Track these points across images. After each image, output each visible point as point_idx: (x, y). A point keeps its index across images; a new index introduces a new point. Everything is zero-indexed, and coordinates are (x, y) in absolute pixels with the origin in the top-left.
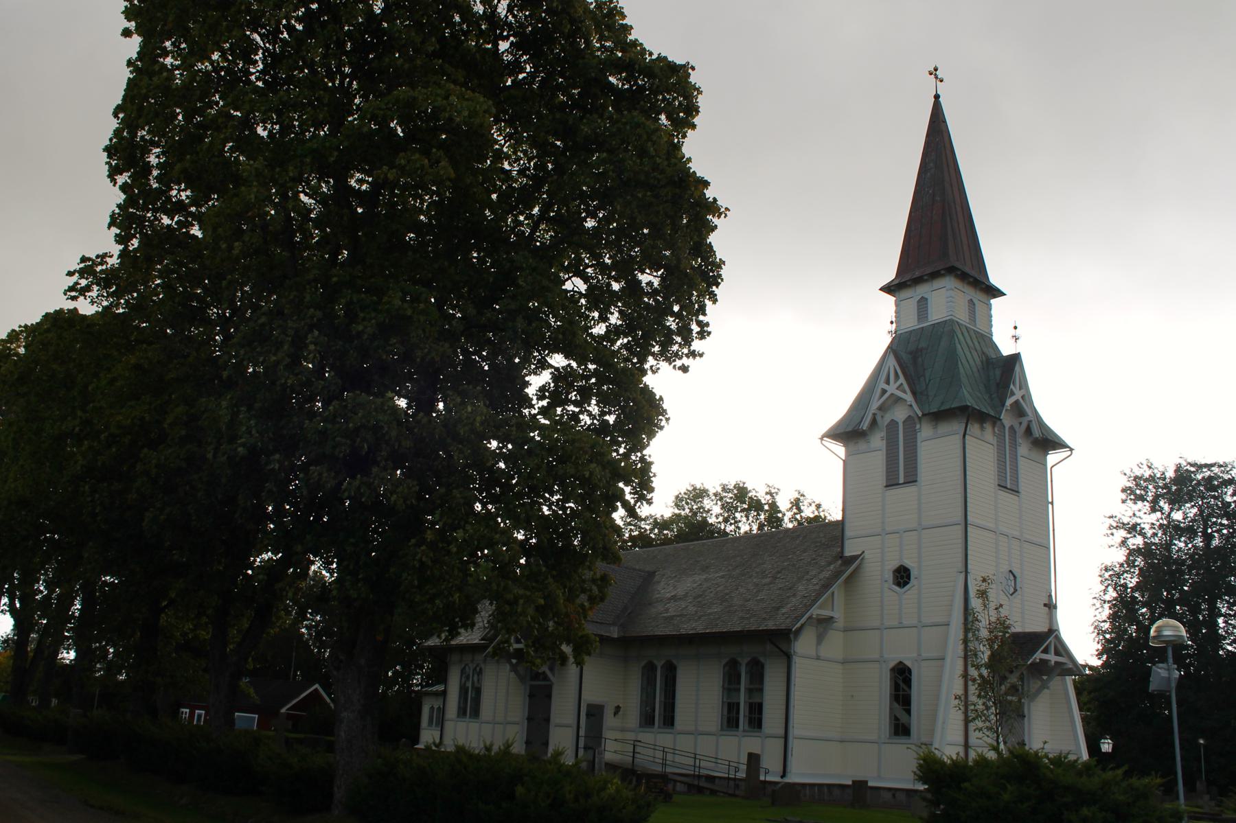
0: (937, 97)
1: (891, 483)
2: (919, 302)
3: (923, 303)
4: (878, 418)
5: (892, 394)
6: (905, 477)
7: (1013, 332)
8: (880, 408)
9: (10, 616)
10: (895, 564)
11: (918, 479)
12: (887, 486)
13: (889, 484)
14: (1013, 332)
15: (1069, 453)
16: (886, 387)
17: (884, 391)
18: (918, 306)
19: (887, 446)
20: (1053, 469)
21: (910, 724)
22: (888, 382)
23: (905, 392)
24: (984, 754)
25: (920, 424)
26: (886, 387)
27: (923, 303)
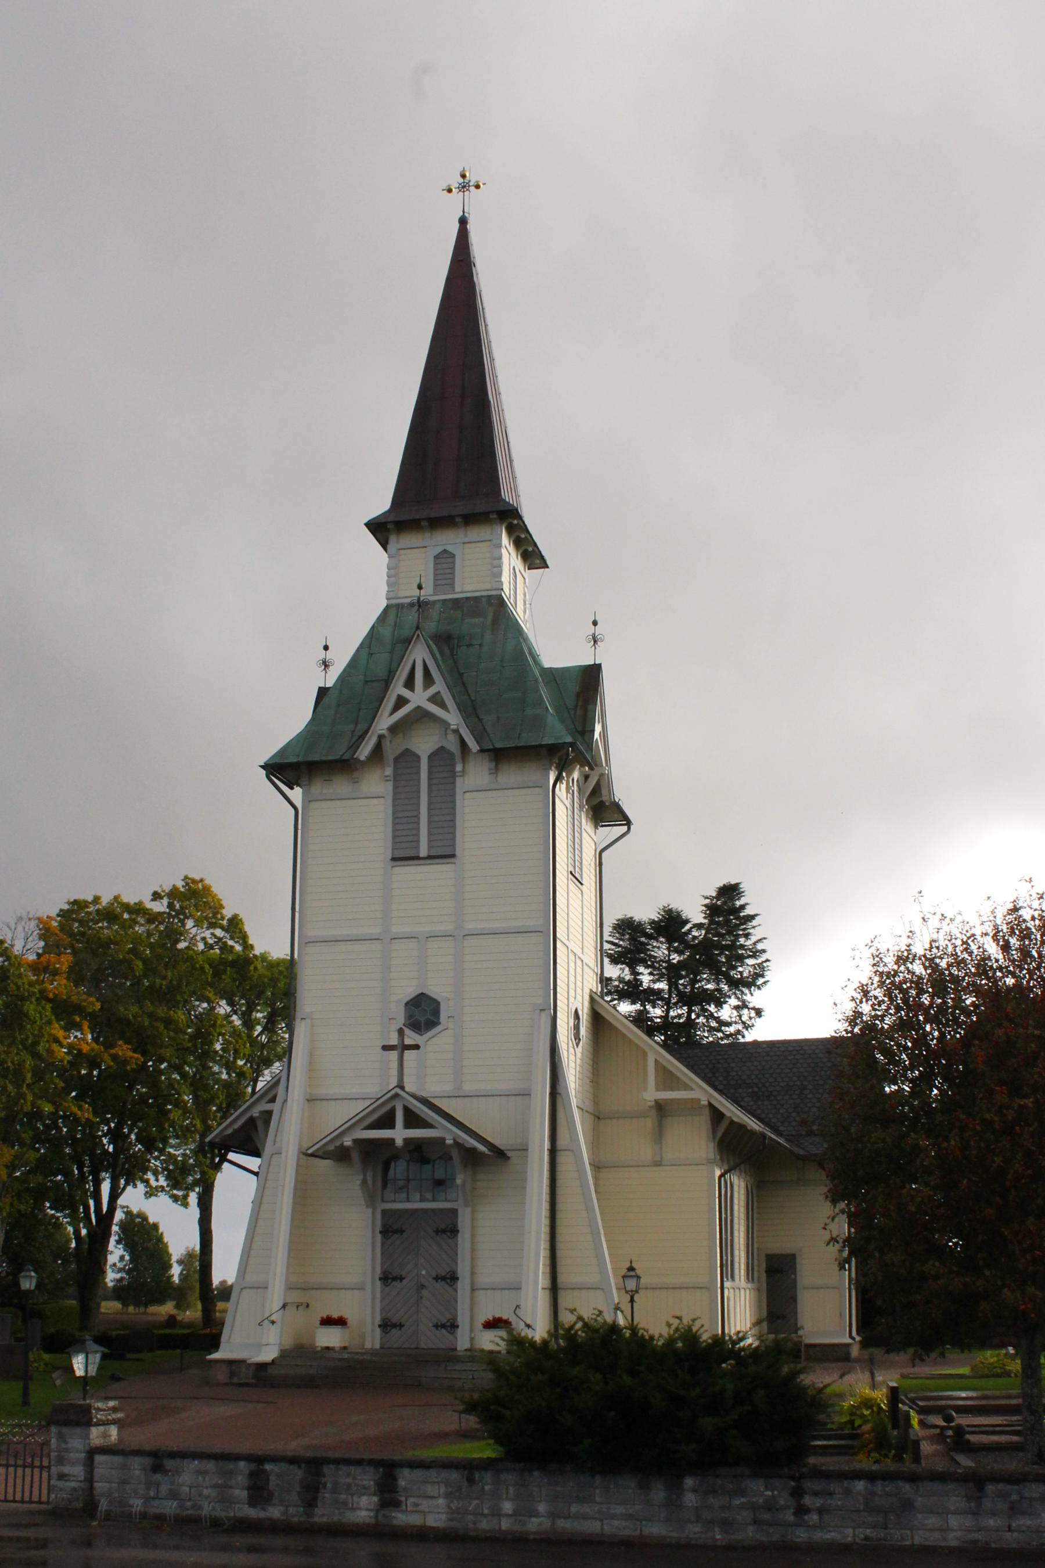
0: (463, 221)
1: (402, 856)
2: (436, 557)
3: (445, 561)
4: (387, 745)
5: (419, 707)
6: (430, 847)
7: (322, 654)
8: (394, 729)
9: (171, 1250)
10: (410, 992)
11: (457, 853)
12: (394, 859)
13: (398, 855)
14: (322, 654)
15: (625, 828)
16: (406, 693)
17: (401, 702)
18: (436, 564)
19: (395, 793)
20: (604, 854)
21: (457, 1270)
22: (410, 684)
23: (443, 705)
24: (694, 1329)
25: (464, 763)
26: (406, 693)
27: (445, 561)
